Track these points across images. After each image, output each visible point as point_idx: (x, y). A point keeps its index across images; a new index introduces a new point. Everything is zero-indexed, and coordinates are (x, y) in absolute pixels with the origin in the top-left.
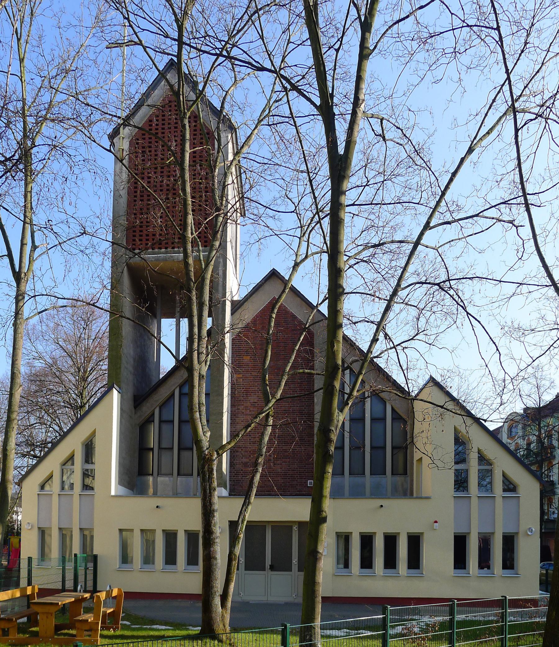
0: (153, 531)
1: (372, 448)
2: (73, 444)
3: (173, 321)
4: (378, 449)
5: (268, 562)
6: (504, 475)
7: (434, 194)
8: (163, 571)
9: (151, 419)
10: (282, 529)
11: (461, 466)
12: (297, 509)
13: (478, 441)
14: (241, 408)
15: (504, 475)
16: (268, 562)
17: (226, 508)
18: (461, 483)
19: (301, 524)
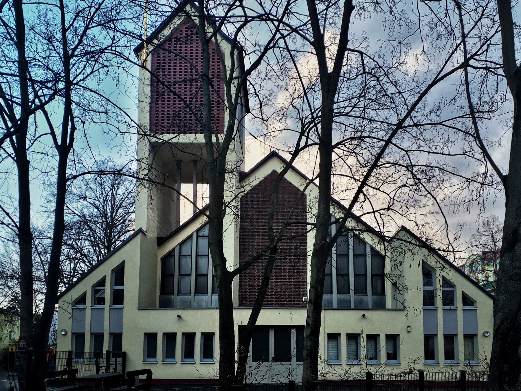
0: (175, 335)
1: (355, 275)
2: (105, 271)
3: (191, 186)
4: (360, 276)
5: (272, 354)
6: (463, 293)
7: (439, 149)
8: (183, 363)
9: (173, 254)
10: (283, 331)
11: (428, 288)
12: (299, 317)
13: (441, 272)
14: (248, 246)
15: (463, 293)
16: (272, 354)
17: (241, 317)
18: (429, 299)
19: (299, 328)
